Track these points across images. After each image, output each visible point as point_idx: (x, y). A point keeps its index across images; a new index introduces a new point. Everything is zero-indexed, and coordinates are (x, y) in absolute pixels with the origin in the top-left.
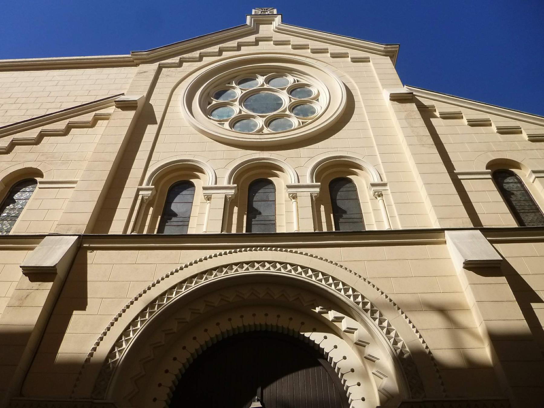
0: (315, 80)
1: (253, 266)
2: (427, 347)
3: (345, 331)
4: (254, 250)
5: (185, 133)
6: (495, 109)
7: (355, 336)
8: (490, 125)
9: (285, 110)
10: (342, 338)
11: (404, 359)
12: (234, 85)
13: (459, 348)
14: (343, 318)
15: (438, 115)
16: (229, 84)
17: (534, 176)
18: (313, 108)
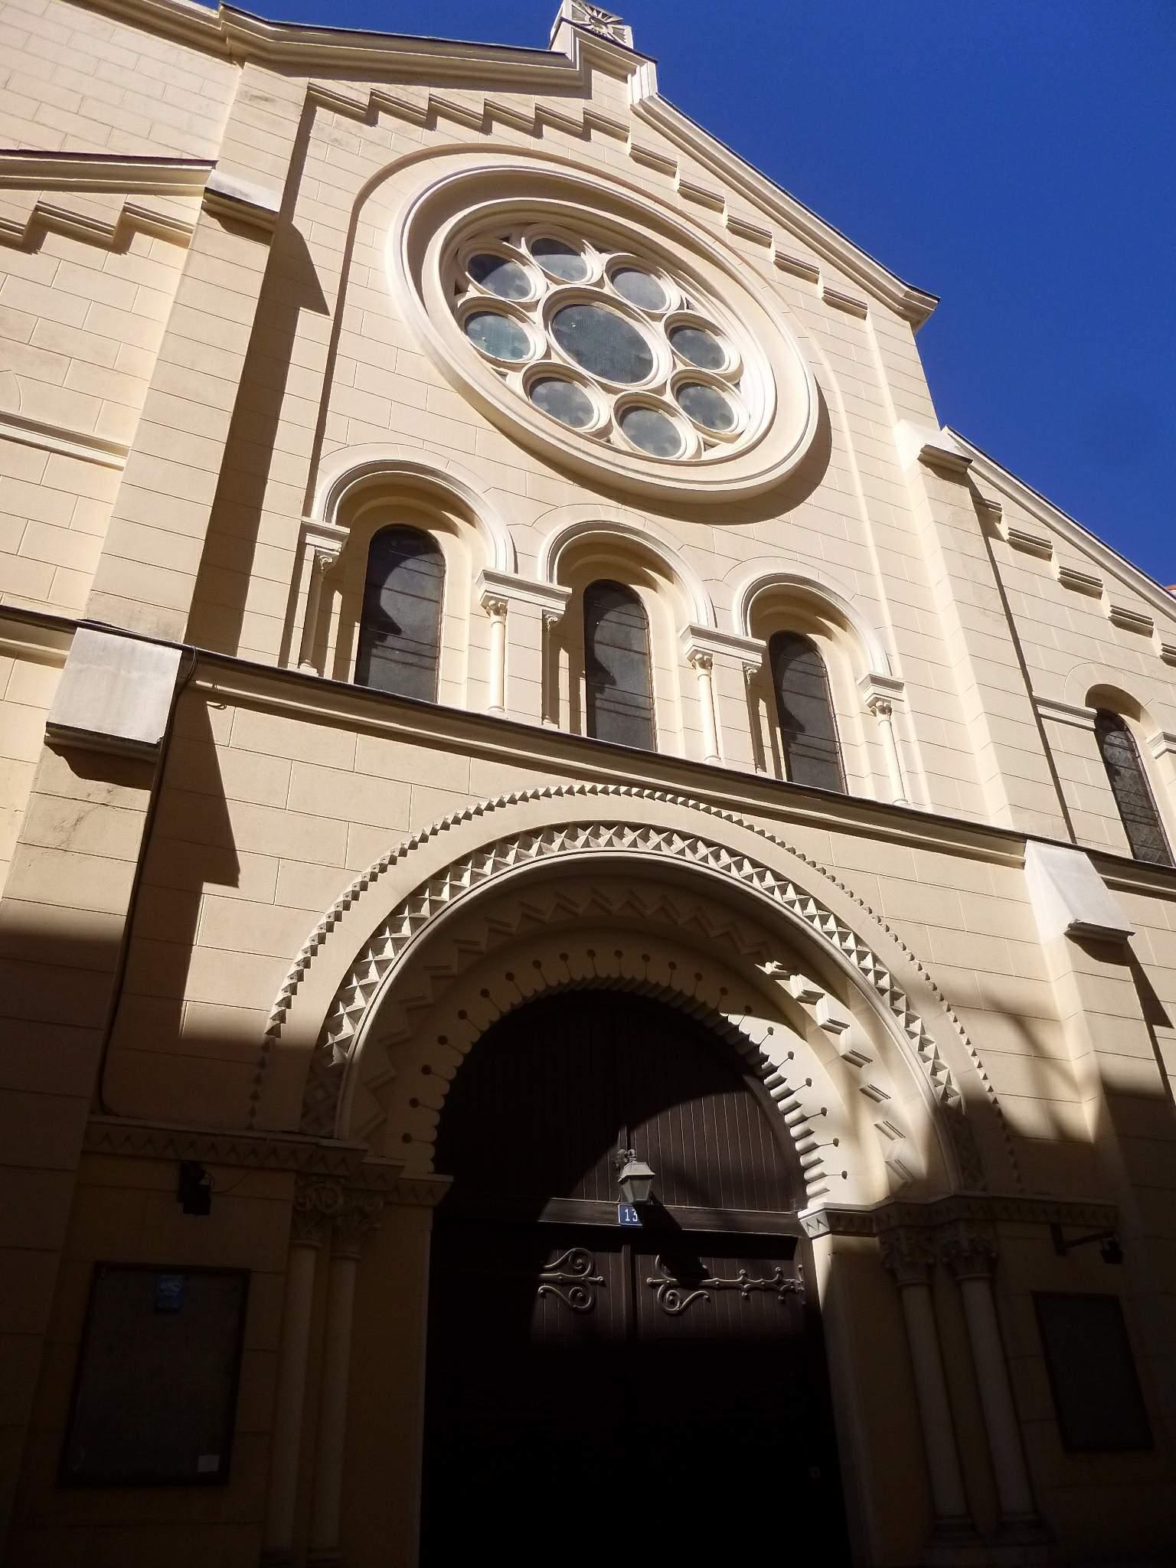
0: (736, 322)
1: (645, 838)
2: (991, 1090)
3: (824, 1027)
4: (660, 798)
5: (402, 374)
6: (1114, 560)
7: (843, 1042)
8: (1099, 595)
9: (660, 390)
10: (803, 1037)
11: (949, 1108)
12: (524, 250)
13: (1044, 1097)
14: (821, 996)
15: (1006, 536)
16: (507, 239)
17: (1164, 745)
18: (723, 404)
